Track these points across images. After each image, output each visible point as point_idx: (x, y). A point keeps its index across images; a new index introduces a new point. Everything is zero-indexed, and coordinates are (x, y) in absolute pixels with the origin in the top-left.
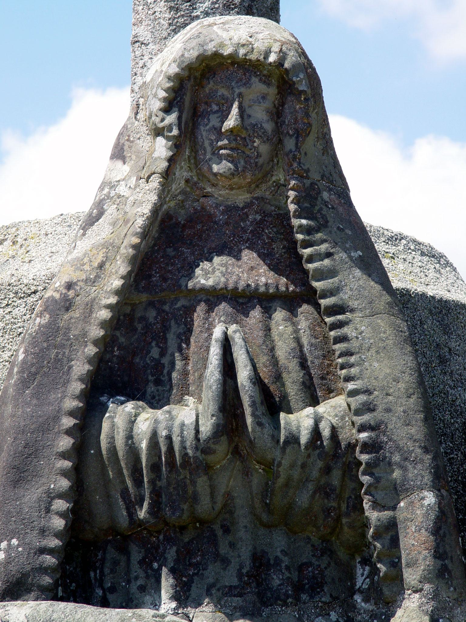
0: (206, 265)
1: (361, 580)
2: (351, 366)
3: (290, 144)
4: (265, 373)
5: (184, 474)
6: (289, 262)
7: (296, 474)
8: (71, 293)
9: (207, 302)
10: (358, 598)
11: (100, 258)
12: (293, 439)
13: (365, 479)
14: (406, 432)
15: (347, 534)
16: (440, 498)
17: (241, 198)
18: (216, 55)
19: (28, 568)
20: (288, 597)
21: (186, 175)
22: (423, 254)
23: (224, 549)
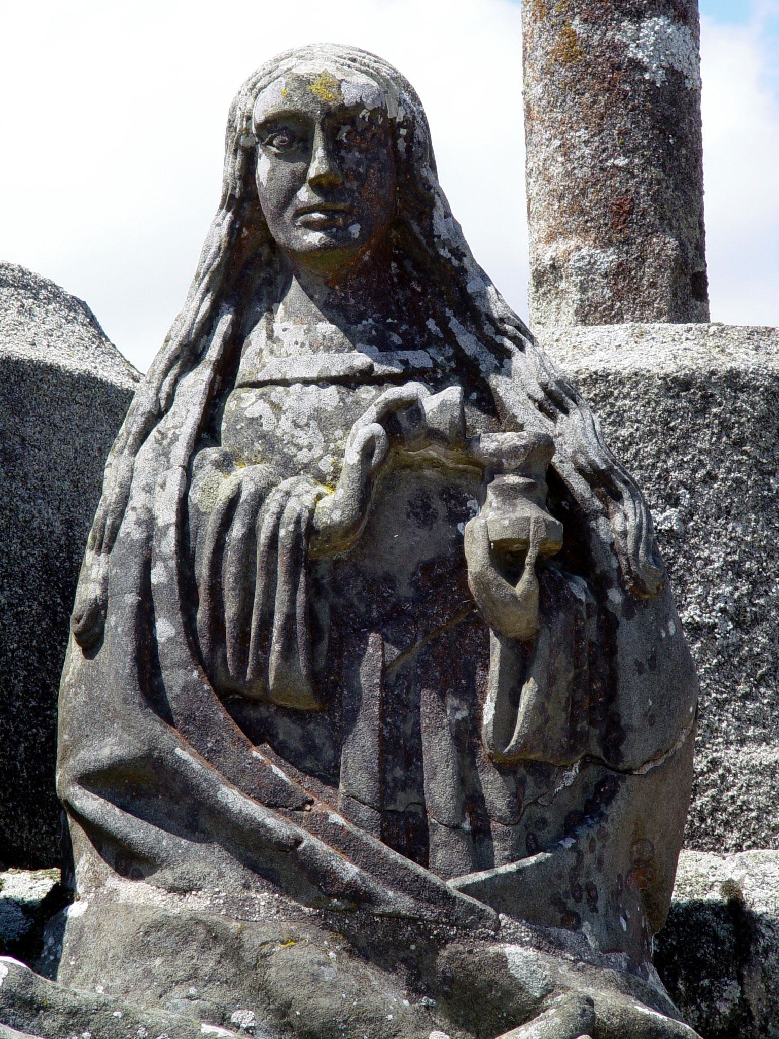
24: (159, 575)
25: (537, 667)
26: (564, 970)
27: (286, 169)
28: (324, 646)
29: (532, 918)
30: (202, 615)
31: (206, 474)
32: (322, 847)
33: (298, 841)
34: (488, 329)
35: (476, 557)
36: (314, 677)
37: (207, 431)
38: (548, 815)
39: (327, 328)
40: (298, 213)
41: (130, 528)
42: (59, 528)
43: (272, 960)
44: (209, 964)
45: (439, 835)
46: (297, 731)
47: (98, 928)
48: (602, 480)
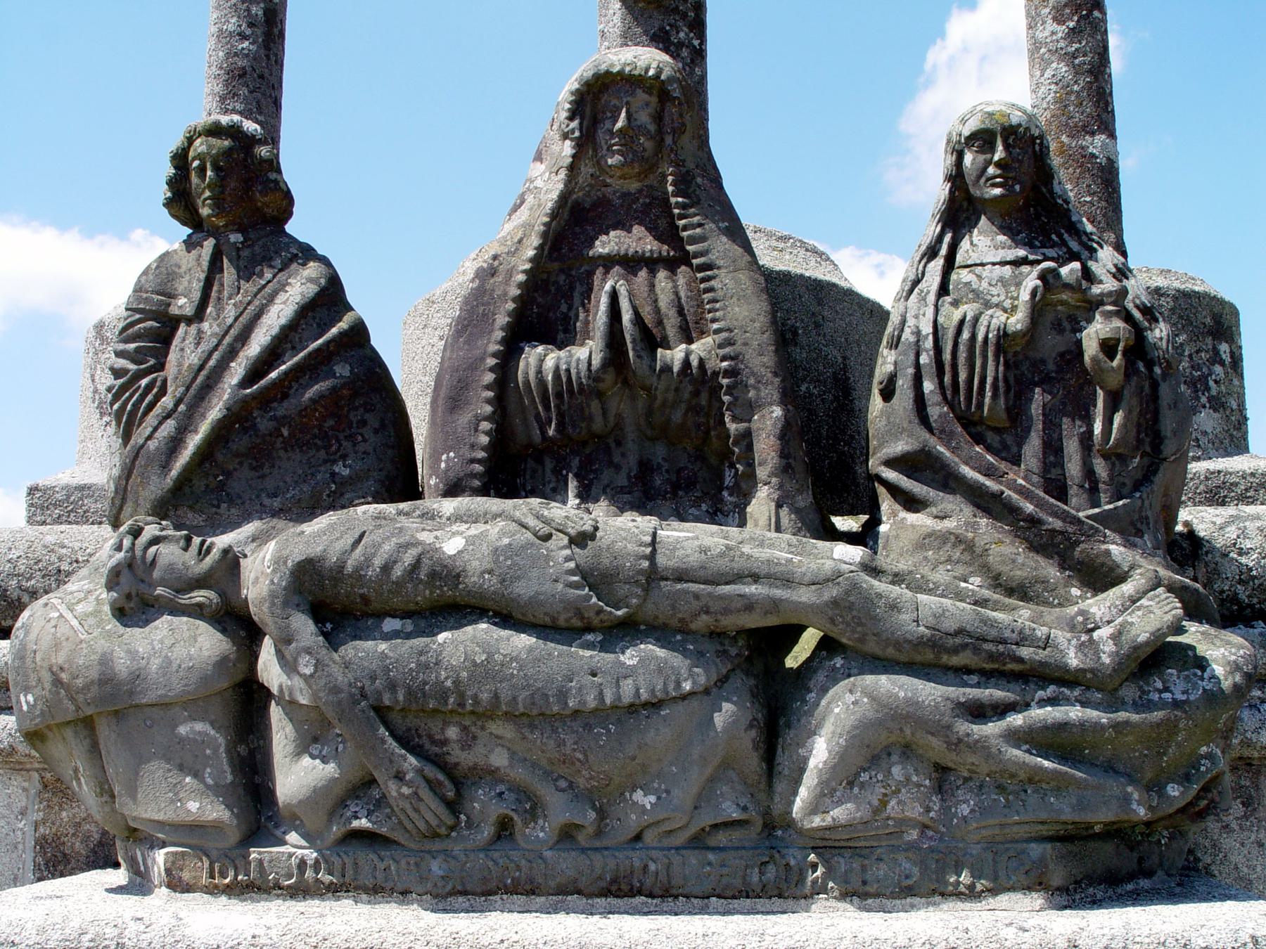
0: (604, 238)
1: (728, 481)
2: (717, 310)
3: (669, 140)
4: (649, 319)
5: (581, 399)
6: (669, 234)
7: (671, 396)
8: (496, 263)
9: (605, 266)
10: (725, 493)
11: (519, 235)
12: (667, 369)
13: (726, 398)
14: (760, 359)
15: (715, 443)
16: (787, 411)
17: (634, 186)
18: (608, 73)
19: (462, 474)
20: (667, 493)
21: (591, 171)
22: (807, 250)
23: (617, 459)
24: (924, 359)
25: (1124, 404)
26: (1138, 557)
27: (981, 158)
28: (1012, 394)
29: (1121, 532)
30: (947, 379)
31: (946, 308)
32: (1015, 496)
33: (1002, 493)
34: (1084, 238)
35: (1091, 348)
36: (1008, 410)
37: (943, 290)
38: (1127, 481)
39: (1002, 238)
40: (988, 180)
41: (907, 335)
42: (840, 360)
43: (991, 552)
44: (957, 554)
45: (1073, 490)
46: (997, 438)
47: (897, 536)
48: (1147, 311)
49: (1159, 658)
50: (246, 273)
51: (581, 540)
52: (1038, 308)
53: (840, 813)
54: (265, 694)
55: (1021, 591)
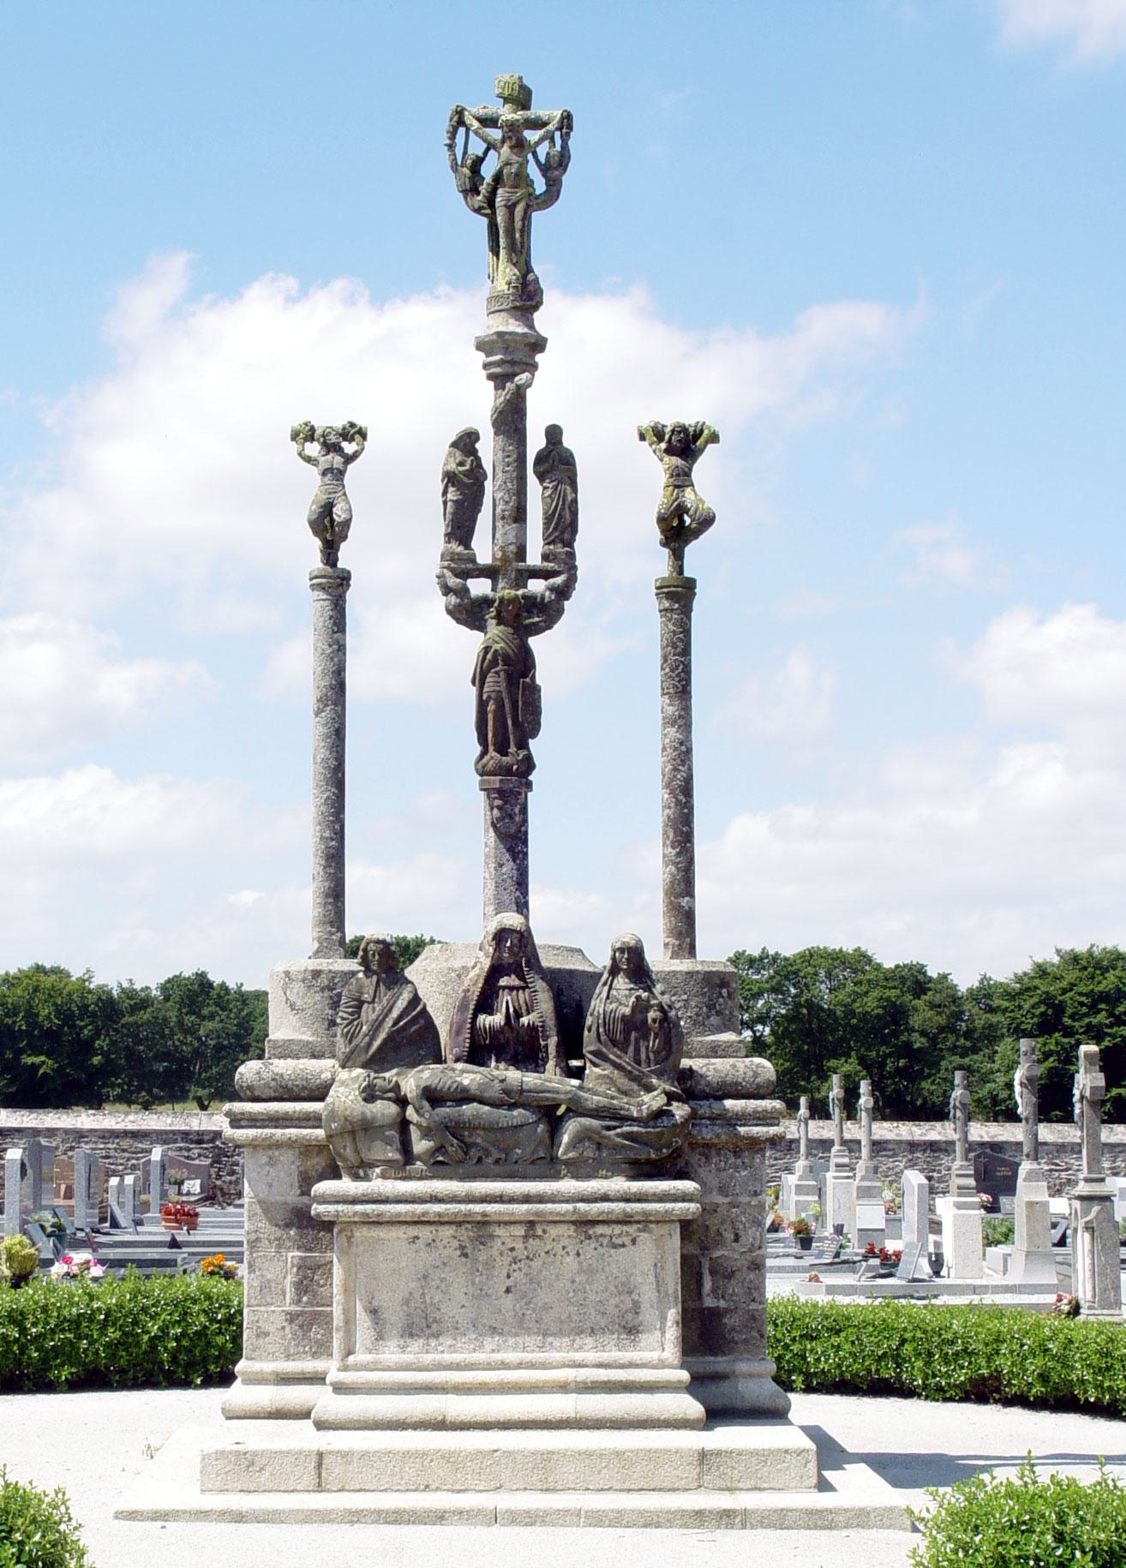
14: (551, 1023)
49: (660, 1114)
50: (389, 988)
51: (502, 1081)
52: (634, 1008)
53: (571, 1155)
54: (409, 1122)
55: (625, 1093)
